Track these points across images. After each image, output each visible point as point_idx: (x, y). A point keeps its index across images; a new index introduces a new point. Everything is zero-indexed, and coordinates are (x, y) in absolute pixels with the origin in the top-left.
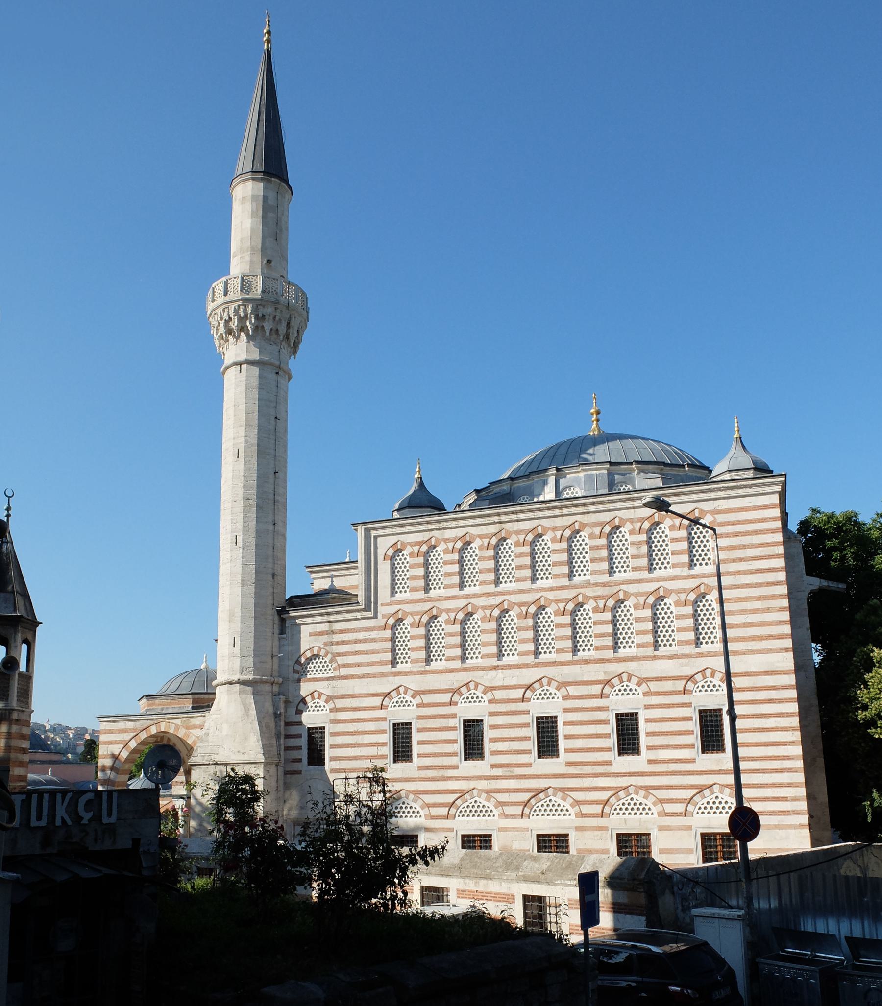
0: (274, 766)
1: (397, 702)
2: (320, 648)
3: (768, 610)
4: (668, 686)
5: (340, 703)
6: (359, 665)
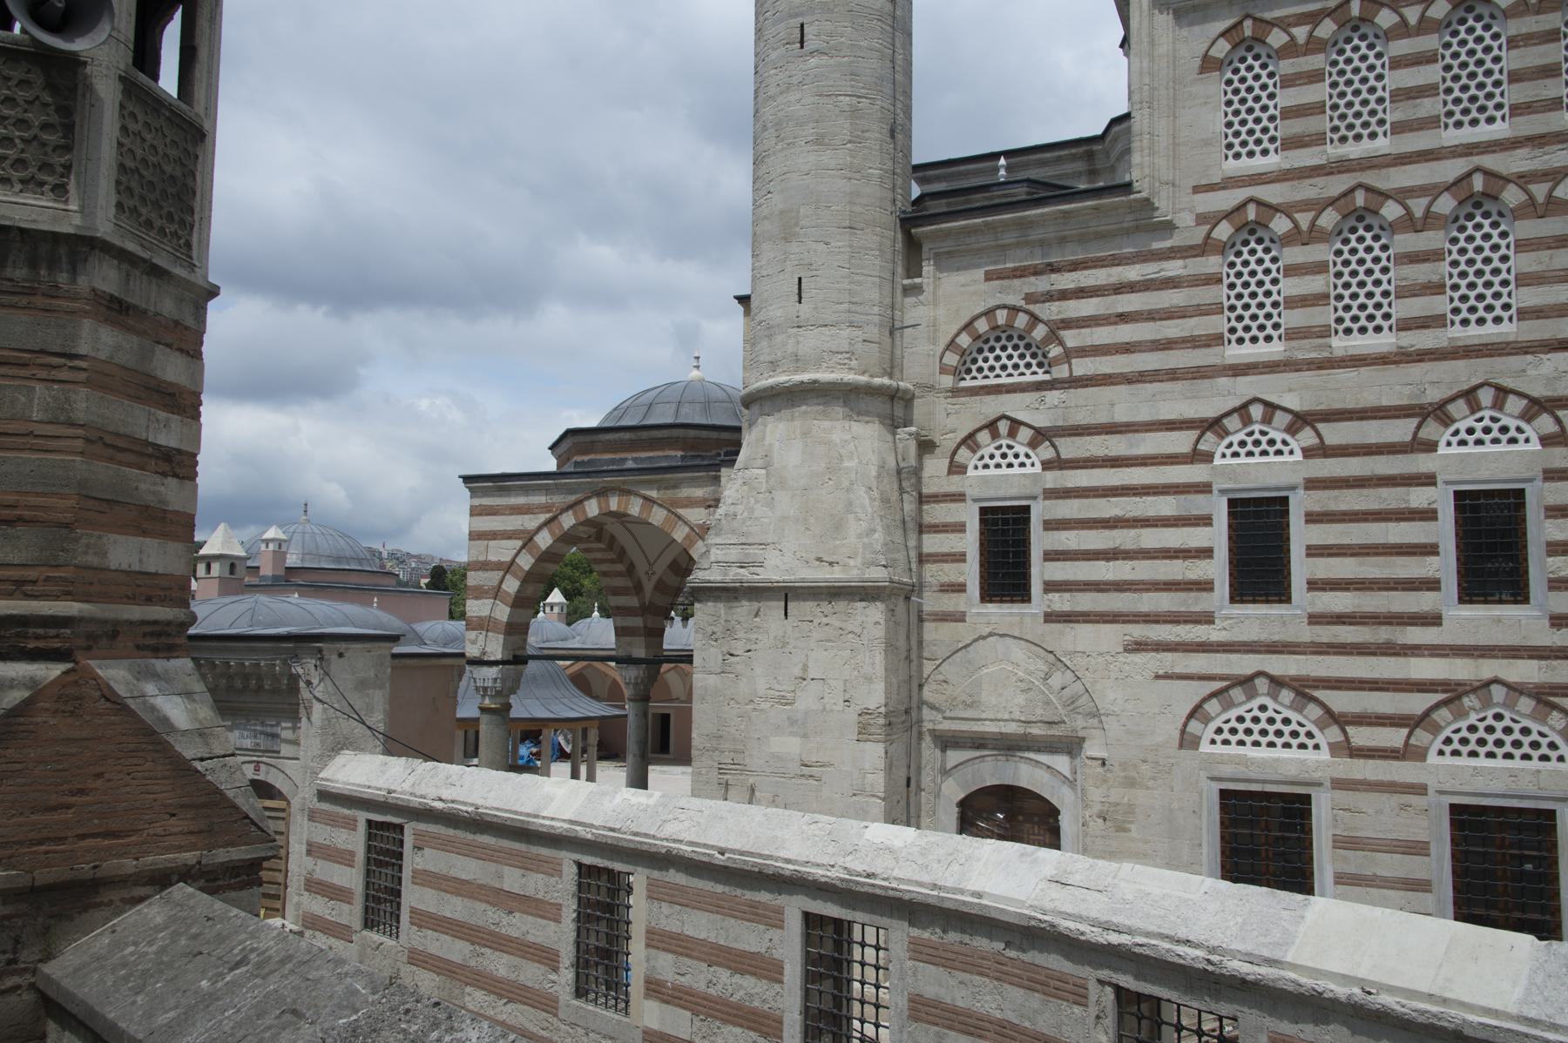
0: (901, 599)
1: (1242, 444)
2: (1014, 310)
4: (1374, 432)
5: (1070, 448)
6: (1127, 348)
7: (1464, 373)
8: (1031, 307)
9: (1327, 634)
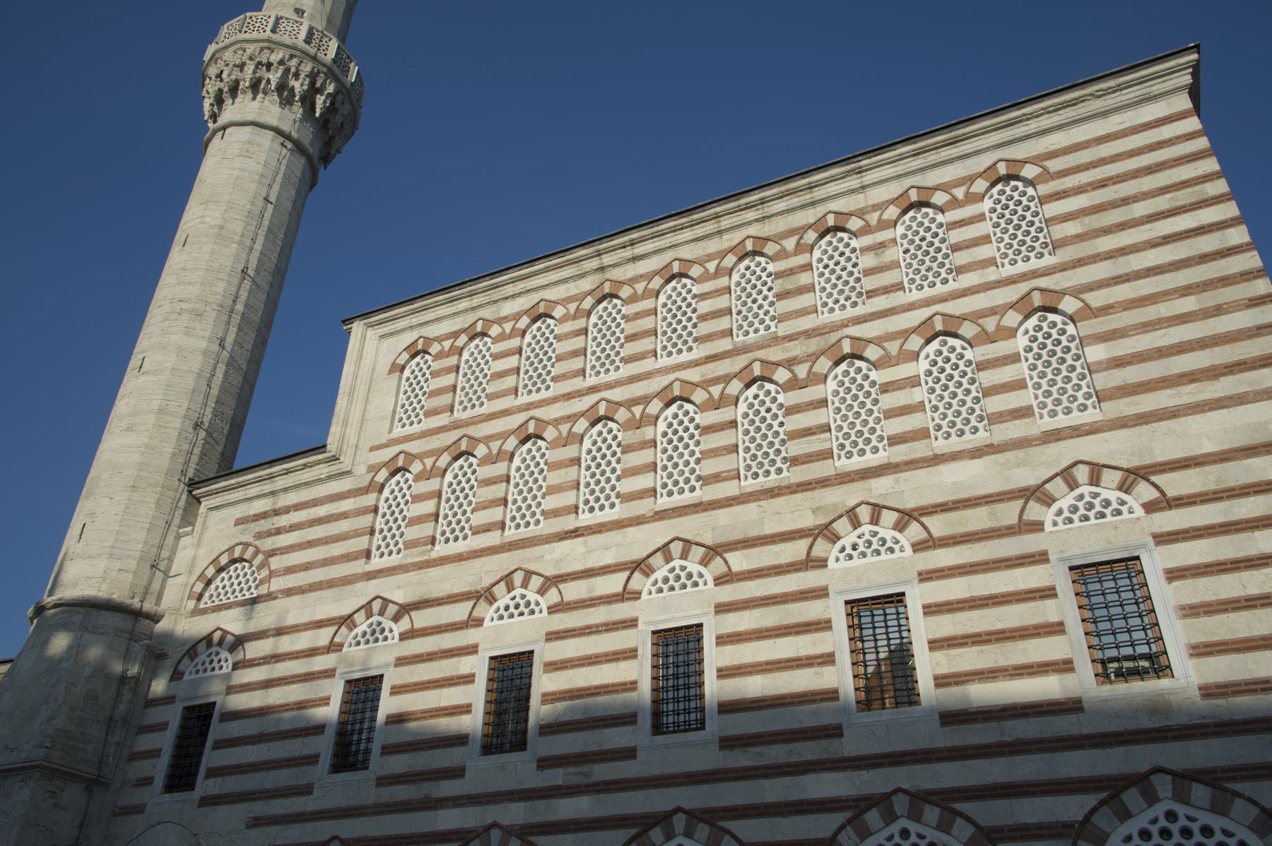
3: (1218, 310)
6: (307, 567)
7: (657, 534)
8: (257, 543)
9: (557, 777)
